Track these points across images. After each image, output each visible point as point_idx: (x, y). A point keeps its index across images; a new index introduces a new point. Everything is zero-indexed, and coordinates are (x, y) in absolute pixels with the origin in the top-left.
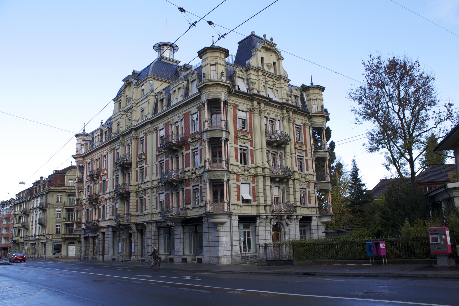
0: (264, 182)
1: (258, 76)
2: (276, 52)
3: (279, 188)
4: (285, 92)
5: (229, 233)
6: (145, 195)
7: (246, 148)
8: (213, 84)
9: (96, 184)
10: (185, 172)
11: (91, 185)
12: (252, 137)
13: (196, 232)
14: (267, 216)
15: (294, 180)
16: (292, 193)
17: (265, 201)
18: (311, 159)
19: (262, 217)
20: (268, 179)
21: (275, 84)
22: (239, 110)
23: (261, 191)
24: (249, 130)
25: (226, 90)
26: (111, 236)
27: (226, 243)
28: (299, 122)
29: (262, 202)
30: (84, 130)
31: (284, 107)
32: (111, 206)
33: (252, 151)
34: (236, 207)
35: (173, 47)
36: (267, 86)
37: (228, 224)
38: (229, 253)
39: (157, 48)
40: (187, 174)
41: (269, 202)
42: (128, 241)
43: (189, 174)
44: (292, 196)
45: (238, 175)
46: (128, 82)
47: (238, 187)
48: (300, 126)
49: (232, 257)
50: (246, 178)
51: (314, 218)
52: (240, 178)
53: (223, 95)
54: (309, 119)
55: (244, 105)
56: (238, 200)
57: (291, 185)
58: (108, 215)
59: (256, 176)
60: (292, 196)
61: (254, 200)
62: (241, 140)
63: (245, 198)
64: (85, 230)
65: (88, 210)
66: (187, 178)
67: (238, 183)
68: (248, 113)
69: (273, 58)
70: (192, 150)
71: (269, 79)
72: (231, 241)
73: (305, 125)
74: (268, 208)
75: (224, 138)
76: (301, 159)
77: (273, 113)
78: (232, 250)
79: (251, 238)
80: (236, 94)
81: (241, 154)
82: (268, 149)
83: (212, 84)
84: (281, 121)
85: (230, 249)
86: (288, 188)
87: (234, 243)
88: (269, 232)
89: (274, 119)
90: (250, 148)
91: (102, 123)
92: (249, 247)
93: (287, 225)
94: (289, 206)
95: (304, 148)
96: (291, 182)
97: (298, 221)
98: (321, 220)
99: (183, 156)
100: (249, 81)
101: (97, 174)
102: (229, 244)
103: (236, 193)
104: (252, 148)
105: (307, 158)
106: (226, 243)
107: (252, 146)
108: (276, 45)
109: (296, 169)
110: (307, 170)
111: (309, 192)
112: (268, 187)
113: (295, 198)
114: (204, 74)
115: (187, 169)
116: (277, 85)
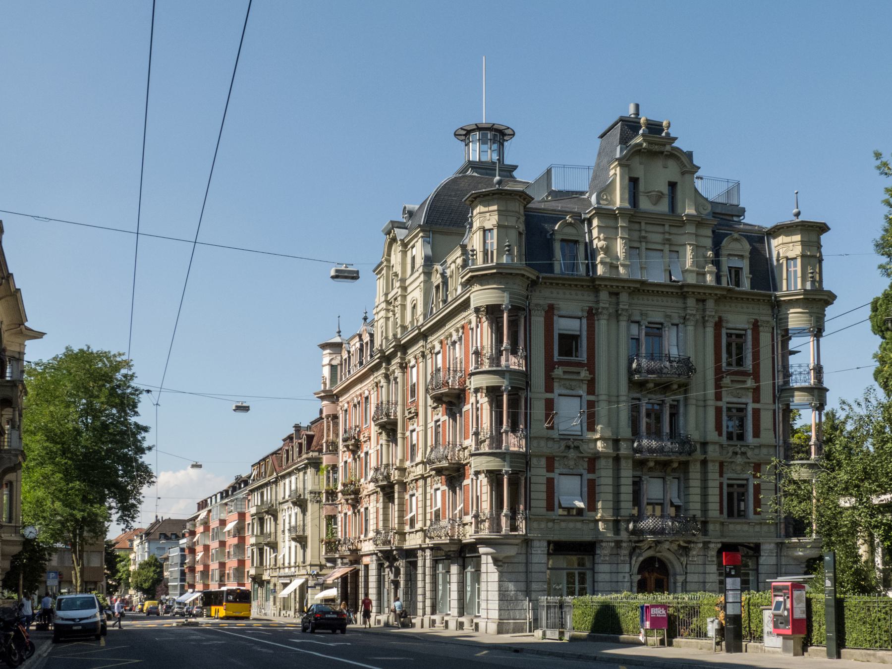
18: (772, 407)
31: (688, 292)
47: (550, 483)
48: (746, 330)
65: (346, 514)
67: (550, 475)
68: (584, 321)
69: (671, 172)
73: (756, 326)
81: (729, 345)
88: (627, 575)
89: (662, 324)
103: (544, 496)
114: (473, 251)
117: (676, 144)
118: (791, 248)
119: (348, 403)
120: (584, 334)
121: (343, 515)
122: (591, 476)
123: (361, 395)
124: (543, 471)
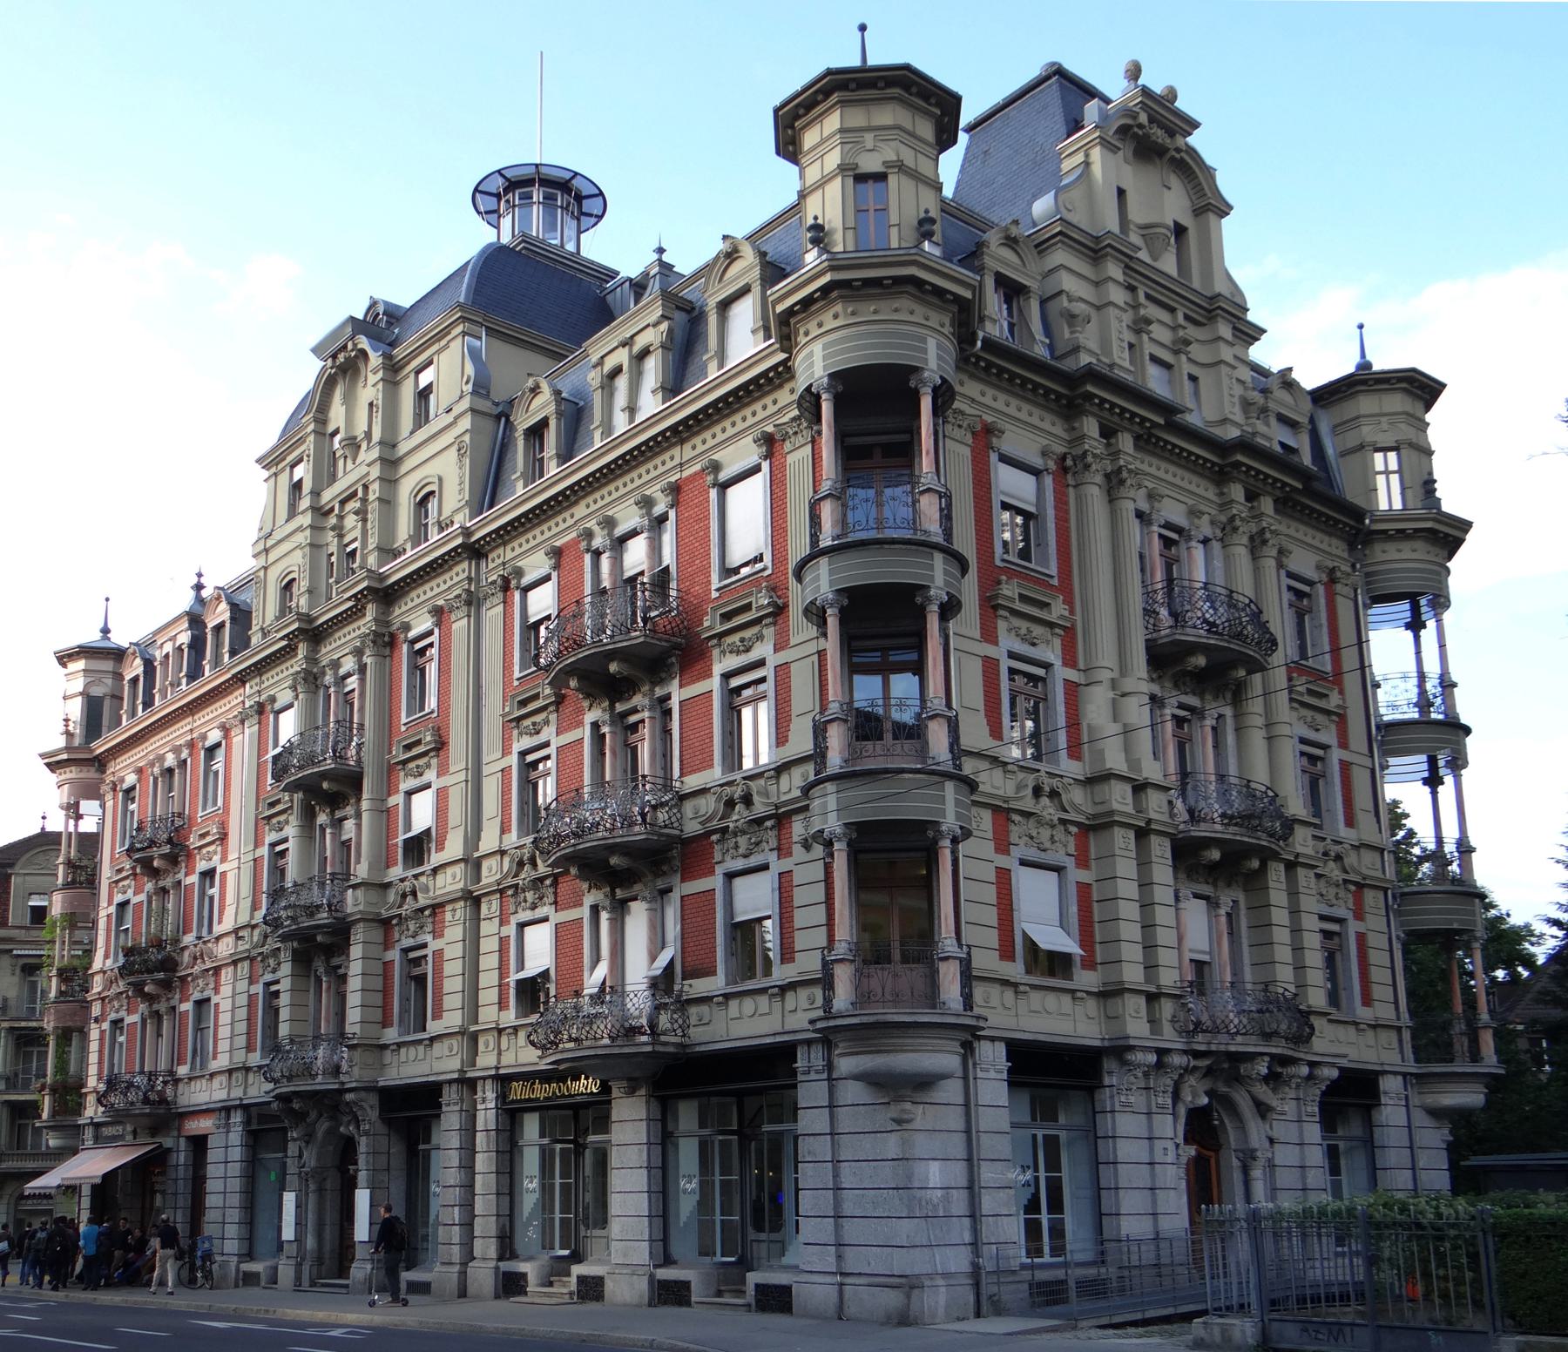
0: (1144, 863)
1: (1097, 284)
2: (1193, 173)
3: (1212, 903)
4: (1238, 390)
5: (959, 1140)
6: (437, 934)
7: (1040, 672)
8: (876, 282)
9: (164, 891)
10: (683, 797)
11: (135, 900)
12: (1072, 612)
13: (747, 1132)
14: (1162, 1052)
15: (1291, 866)
16: (1282, 935)
17: (1151, 967)
18: (1368, 763)
19: (1138, 1057)
20: (1160, 849)
21: (1187, 343)
22: (1005, 459)
23: (1129, 911)
24: (1053, 570)
25: (947, 321)
26: (236, 1154)
27: (946, 1200)
28: (1304, 562)
29: (1133, 974)
30: (105, 631)
31: (1238, 464)
32: (243, 1000)
33: (1072, 689)
34: (995, 990)
35: (579, 198)
36: (1149, 348)
37: (951, 1091)
38: (959, 1261)
39: (491, 203)
40: (688, 807)
41: (1169, 978)
42: (333, 1183)
43: (708, 805)
44: (1283, 953)
45: (1002, 813)
46: (341, 358)
47: (1004, 880)
48: (1310, 583)
49: (977, 1285)
50: (1045, 833)
51: (1391, 1085)
52: (1015, 833)
53: (931, 344)
54: (1352, 547)
55: (1028, 432)
56: (1007, 953)
57: (1278, 896)
58: (224, 1046)
59: (1099, 825)
60: (1283, 953)
61: (1089, 963)
62: (1016, 622)
63: (1044, 944)
64: (97, 1126)
66: (692, 828)
67: (1003, 861)
68: (1048, 480)
69: (1174, 205)
70: (727, 676)
71: (1152, 311)
72: (972, 1188)
73: (1332, 579)
74: (1167, 1008)
75: (938, 592)
76: (1313, 759)
77: (1179, 496)
78: (975, 1245)
79: (1065, 1174)
80: (990, 365)
82: (1155, 689)
83: (867, 282)
84: (1216, 545)
85: (967, 1238)
86: (1261, 907)
87: (988, 1203)
88: (1170, 1145)
90: (1062, 673)
91: (199, 587)
92: (1057, 1232)
93: (1263, 1110)
94: (1270, 1001)
95: (1334, 701)
96: (1276, 873)
97: (1316, 1092)
98: (1430, 1100)
99: (667, 713)
100: (1053, 306)
101: (170, 841)
102: (959, 1203)
103: (991, 916)
104: (1072, 675)
105: (1346, 755)
106: (946, 1200)
107: (1070, 660)
108: (1195, 125)
109: (1296, 806)
110: (1350, 822)
111: (1361, 938)
112: (1163, 894)
113: (1299, 968)
115: (693, 782)
116: (1196, 351)
117: (1194, 140)
118: (1385, 426)
119: (140, 771)
120: (1050, 513)
121: (106, 1026)
122: (1085, 876)
123: (191, 745)
124: (987, 849)
